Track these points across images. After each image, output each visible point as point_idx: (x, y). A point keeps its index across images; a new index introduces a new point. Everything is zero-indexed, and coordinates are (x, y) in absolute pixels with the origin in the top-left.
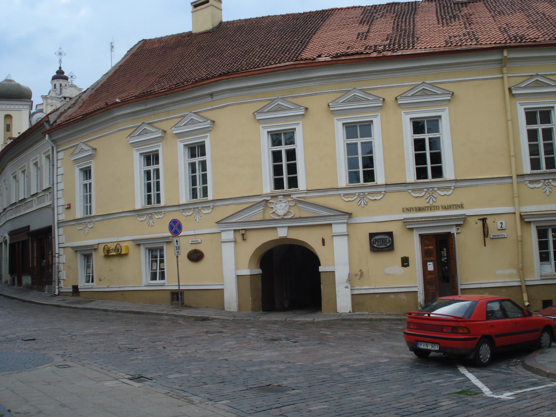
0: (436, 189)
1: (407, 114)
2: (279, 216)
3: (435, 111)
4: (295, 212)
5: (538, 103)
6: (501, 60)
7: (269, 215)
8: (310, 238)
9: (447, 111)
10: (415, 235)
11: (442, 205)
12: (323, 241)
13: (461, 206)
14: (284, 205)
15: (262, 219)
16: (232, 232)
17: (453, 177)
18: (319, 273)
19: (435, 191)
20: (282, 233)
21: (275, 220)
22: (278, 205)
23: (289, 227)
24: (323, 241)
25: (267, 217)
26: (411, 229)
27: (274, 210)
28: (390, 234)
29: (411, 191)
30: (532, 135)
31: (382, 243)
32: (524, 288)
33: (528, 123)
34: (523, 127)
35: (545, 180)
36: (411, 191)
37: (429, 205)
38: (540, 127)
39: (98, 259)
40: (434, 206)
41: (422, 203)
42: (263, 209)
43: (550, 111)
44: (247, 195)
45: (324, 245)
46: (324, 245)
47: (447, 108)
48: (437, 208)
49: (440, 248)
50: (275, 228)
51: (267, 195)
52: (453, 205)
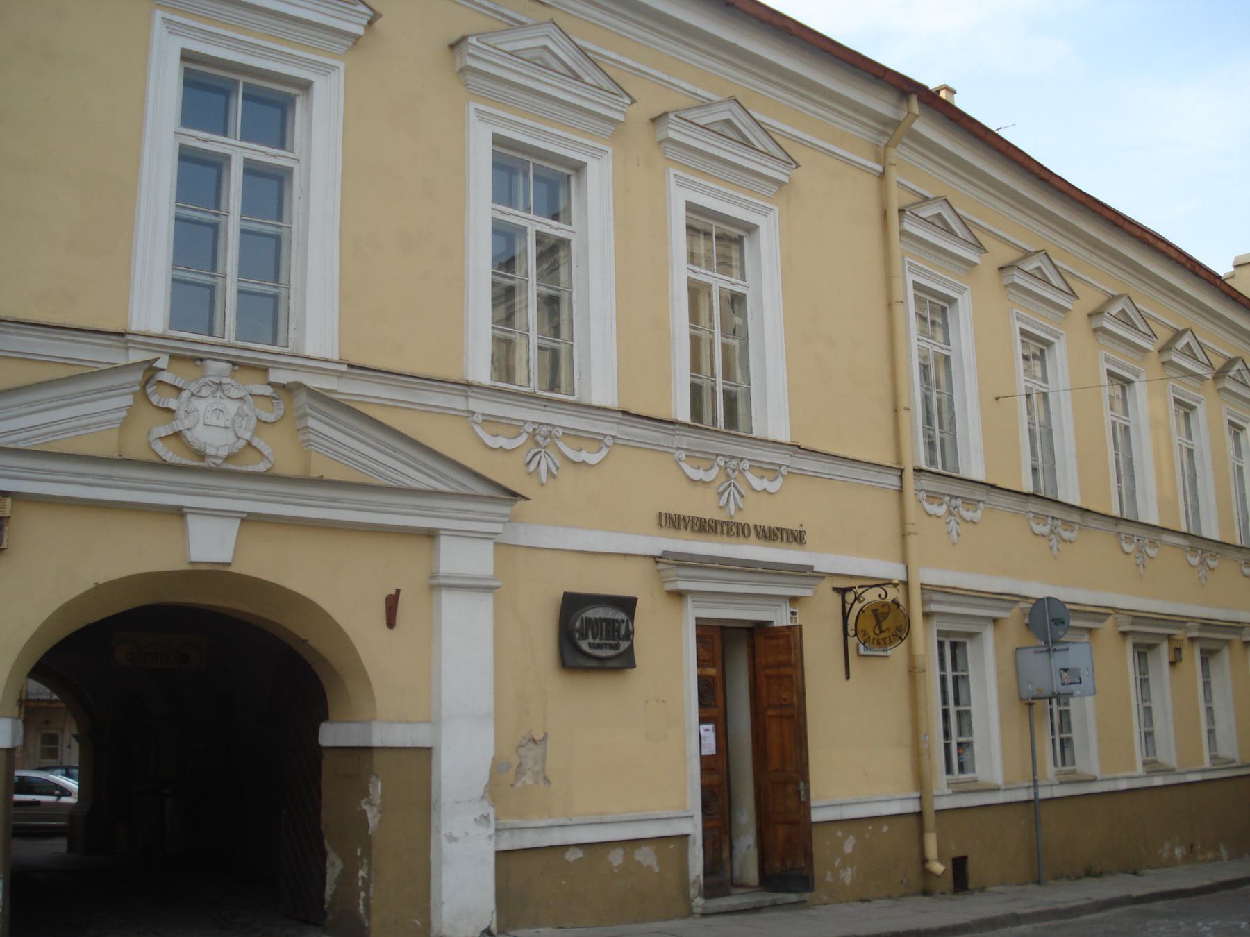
0: (746, 465)
1: (682, 183)
2: (202, 456)
3: (748, 206)
4: (278, 452)
5: (251, 48)
6: (895, 124)
7: (151, 437)
8: (332, 586)
9: (774, 217)
11: (758, 524)
12: (392, 604)
13: (797, 538)
14: (232, 407)
15: (115, 456)
16: (236, 523)
17: (611, 401)
18: (318, 752)
19: (742, 472)
20: (211, 543)
21: (163, 466)
22: (201, 405)
23: (249, 520)
24: (392, 604)
25: (136, 450)
26: (679, 595)
27: (178, 426)
28: (627, 605)
29: (683, 455)
30: (199, 170)
31: (592, 635)
32: (930, 819)
33: (190, 117)
34: (482, 211)
35: (952, 497)
36: (683, 455)
37: (722, 516)
38: (238, 151)
39: (1105, 662)
40: (737, 525)
41: (704, 506)
42: (129, 409)
43: (292, 99)
44: (43, 320)
45: (391, 623)
46: (391, 623)
47: (342, 66)
48: (738, 530)
49: (752, 671)
50: (179, 513)
51: (148, 339)
52: (781, 530)
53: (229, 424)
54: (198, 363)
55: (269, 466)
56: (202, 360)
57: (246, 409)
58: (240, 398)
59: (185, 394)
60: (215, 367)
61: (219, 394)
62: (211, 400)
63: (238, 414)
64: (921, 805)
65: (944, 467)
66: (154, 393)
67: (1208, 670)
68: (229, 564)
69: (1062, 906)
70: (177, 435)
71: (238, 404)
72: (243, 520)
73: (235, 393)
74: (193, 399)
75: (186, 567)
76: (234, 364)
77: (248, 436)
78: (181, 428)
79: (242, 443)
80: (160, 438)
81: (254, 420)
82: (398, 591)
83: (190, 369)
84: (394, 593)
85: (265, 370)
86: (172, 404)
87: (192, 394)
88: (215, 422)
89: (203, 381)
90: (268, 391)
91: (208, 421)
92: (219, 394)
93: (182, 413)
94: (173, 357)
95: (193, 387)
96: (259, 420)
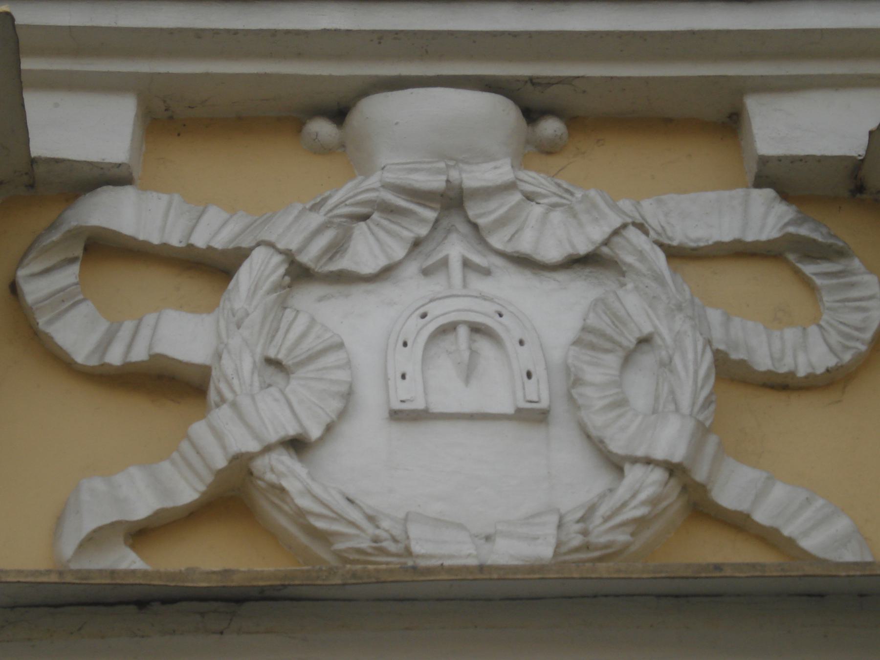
14: (553, 312)
53: (539, 393)
57: (637, 309)
58: (576, 263)
59: (258, 272)
60: (427, 127)
61: (455, 249)
62: (411, 289)
63: (589, 339)
64: (321, 439)
66: (64, 301)
69: (608, 513)
71: (576, 296)
73: (554, 235)
74: (307, 298)
77: (670, 440)
78: (243, 442)
79: (645, 483)
81: (691, 374)
83: (269, 166)
85: (730, 124)
86: (181, 334)
87: (299, 273)
88: (449, 392)
89: (346, 194)
90: (764, 217)
91: (409, 394)
92: (455, 249)
93: (237, 370)
94: (169, 119)
95: (297, 230)
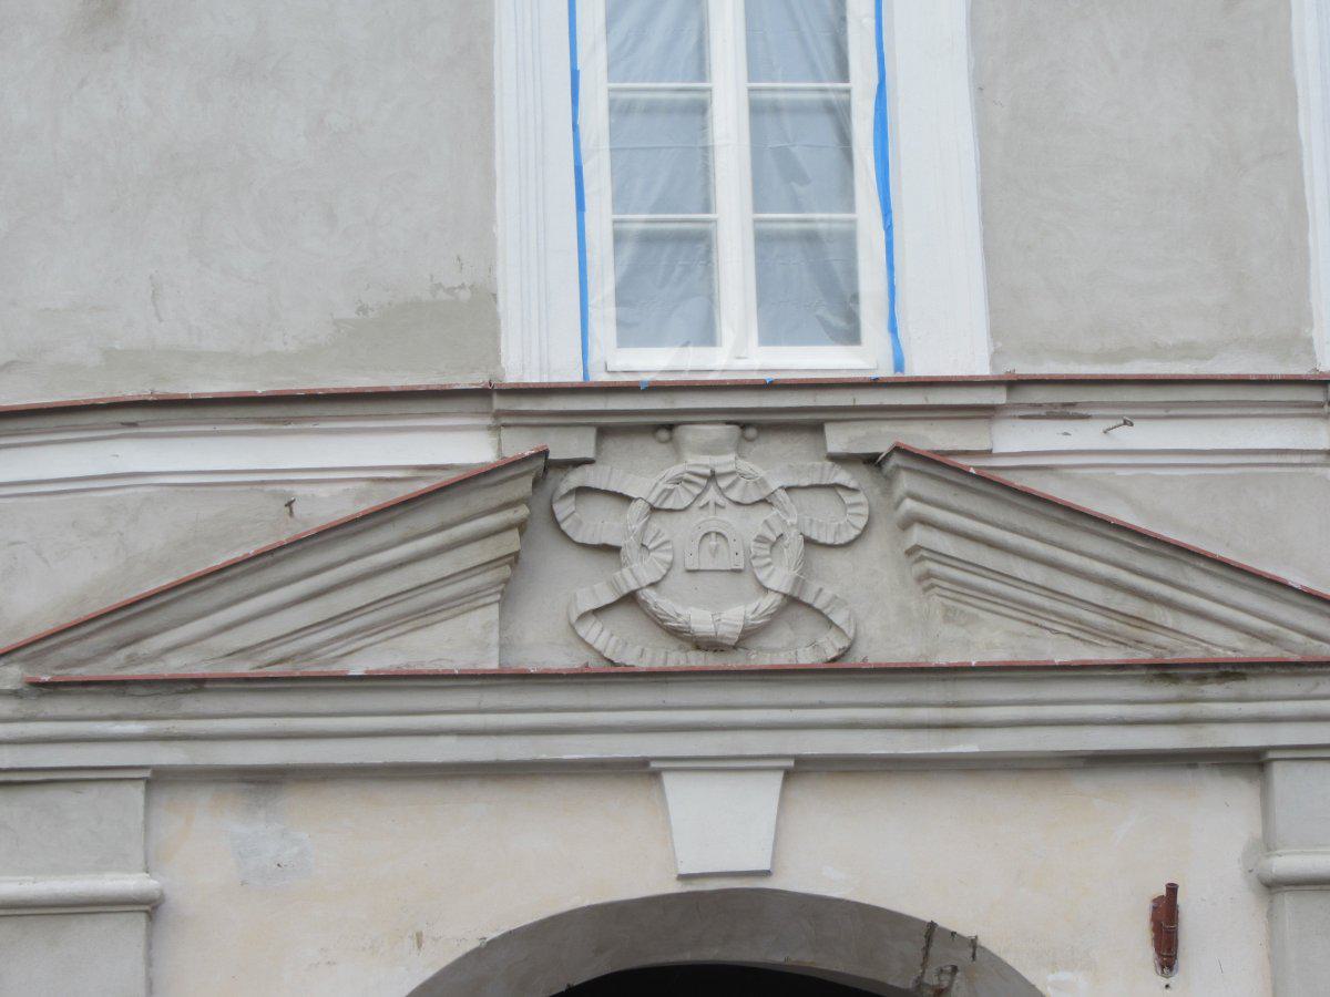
10: (1287, 902)
20: (716, 831)
21: (613, 675)
22: (679, 532)
23: (800, 769)
50: (642, 771)
54: (664, 435)
55: (841, 644)
56: (670, 427)
65: (812, 275)
67: (894, 356)
68: (766, 874)
70: (630, 599)
72: (148, 782)
74: (657, 523)
75: (674, 888)
76: (744, 426)
78: (633, 586)
80: (596, 612)
82: (1172, 890)
84: (1163, 892)
87: (654, 510)
91: (692, 564)
93: (631, 552)
94: (603, 432)
96: (808, 541)
